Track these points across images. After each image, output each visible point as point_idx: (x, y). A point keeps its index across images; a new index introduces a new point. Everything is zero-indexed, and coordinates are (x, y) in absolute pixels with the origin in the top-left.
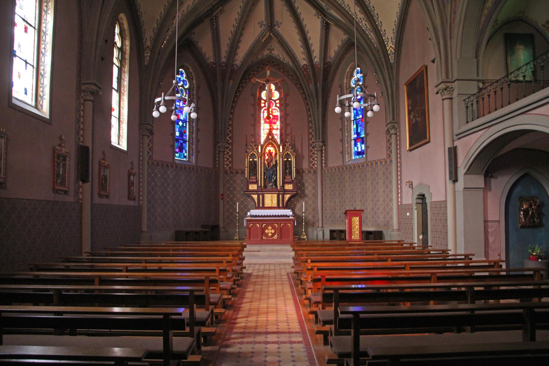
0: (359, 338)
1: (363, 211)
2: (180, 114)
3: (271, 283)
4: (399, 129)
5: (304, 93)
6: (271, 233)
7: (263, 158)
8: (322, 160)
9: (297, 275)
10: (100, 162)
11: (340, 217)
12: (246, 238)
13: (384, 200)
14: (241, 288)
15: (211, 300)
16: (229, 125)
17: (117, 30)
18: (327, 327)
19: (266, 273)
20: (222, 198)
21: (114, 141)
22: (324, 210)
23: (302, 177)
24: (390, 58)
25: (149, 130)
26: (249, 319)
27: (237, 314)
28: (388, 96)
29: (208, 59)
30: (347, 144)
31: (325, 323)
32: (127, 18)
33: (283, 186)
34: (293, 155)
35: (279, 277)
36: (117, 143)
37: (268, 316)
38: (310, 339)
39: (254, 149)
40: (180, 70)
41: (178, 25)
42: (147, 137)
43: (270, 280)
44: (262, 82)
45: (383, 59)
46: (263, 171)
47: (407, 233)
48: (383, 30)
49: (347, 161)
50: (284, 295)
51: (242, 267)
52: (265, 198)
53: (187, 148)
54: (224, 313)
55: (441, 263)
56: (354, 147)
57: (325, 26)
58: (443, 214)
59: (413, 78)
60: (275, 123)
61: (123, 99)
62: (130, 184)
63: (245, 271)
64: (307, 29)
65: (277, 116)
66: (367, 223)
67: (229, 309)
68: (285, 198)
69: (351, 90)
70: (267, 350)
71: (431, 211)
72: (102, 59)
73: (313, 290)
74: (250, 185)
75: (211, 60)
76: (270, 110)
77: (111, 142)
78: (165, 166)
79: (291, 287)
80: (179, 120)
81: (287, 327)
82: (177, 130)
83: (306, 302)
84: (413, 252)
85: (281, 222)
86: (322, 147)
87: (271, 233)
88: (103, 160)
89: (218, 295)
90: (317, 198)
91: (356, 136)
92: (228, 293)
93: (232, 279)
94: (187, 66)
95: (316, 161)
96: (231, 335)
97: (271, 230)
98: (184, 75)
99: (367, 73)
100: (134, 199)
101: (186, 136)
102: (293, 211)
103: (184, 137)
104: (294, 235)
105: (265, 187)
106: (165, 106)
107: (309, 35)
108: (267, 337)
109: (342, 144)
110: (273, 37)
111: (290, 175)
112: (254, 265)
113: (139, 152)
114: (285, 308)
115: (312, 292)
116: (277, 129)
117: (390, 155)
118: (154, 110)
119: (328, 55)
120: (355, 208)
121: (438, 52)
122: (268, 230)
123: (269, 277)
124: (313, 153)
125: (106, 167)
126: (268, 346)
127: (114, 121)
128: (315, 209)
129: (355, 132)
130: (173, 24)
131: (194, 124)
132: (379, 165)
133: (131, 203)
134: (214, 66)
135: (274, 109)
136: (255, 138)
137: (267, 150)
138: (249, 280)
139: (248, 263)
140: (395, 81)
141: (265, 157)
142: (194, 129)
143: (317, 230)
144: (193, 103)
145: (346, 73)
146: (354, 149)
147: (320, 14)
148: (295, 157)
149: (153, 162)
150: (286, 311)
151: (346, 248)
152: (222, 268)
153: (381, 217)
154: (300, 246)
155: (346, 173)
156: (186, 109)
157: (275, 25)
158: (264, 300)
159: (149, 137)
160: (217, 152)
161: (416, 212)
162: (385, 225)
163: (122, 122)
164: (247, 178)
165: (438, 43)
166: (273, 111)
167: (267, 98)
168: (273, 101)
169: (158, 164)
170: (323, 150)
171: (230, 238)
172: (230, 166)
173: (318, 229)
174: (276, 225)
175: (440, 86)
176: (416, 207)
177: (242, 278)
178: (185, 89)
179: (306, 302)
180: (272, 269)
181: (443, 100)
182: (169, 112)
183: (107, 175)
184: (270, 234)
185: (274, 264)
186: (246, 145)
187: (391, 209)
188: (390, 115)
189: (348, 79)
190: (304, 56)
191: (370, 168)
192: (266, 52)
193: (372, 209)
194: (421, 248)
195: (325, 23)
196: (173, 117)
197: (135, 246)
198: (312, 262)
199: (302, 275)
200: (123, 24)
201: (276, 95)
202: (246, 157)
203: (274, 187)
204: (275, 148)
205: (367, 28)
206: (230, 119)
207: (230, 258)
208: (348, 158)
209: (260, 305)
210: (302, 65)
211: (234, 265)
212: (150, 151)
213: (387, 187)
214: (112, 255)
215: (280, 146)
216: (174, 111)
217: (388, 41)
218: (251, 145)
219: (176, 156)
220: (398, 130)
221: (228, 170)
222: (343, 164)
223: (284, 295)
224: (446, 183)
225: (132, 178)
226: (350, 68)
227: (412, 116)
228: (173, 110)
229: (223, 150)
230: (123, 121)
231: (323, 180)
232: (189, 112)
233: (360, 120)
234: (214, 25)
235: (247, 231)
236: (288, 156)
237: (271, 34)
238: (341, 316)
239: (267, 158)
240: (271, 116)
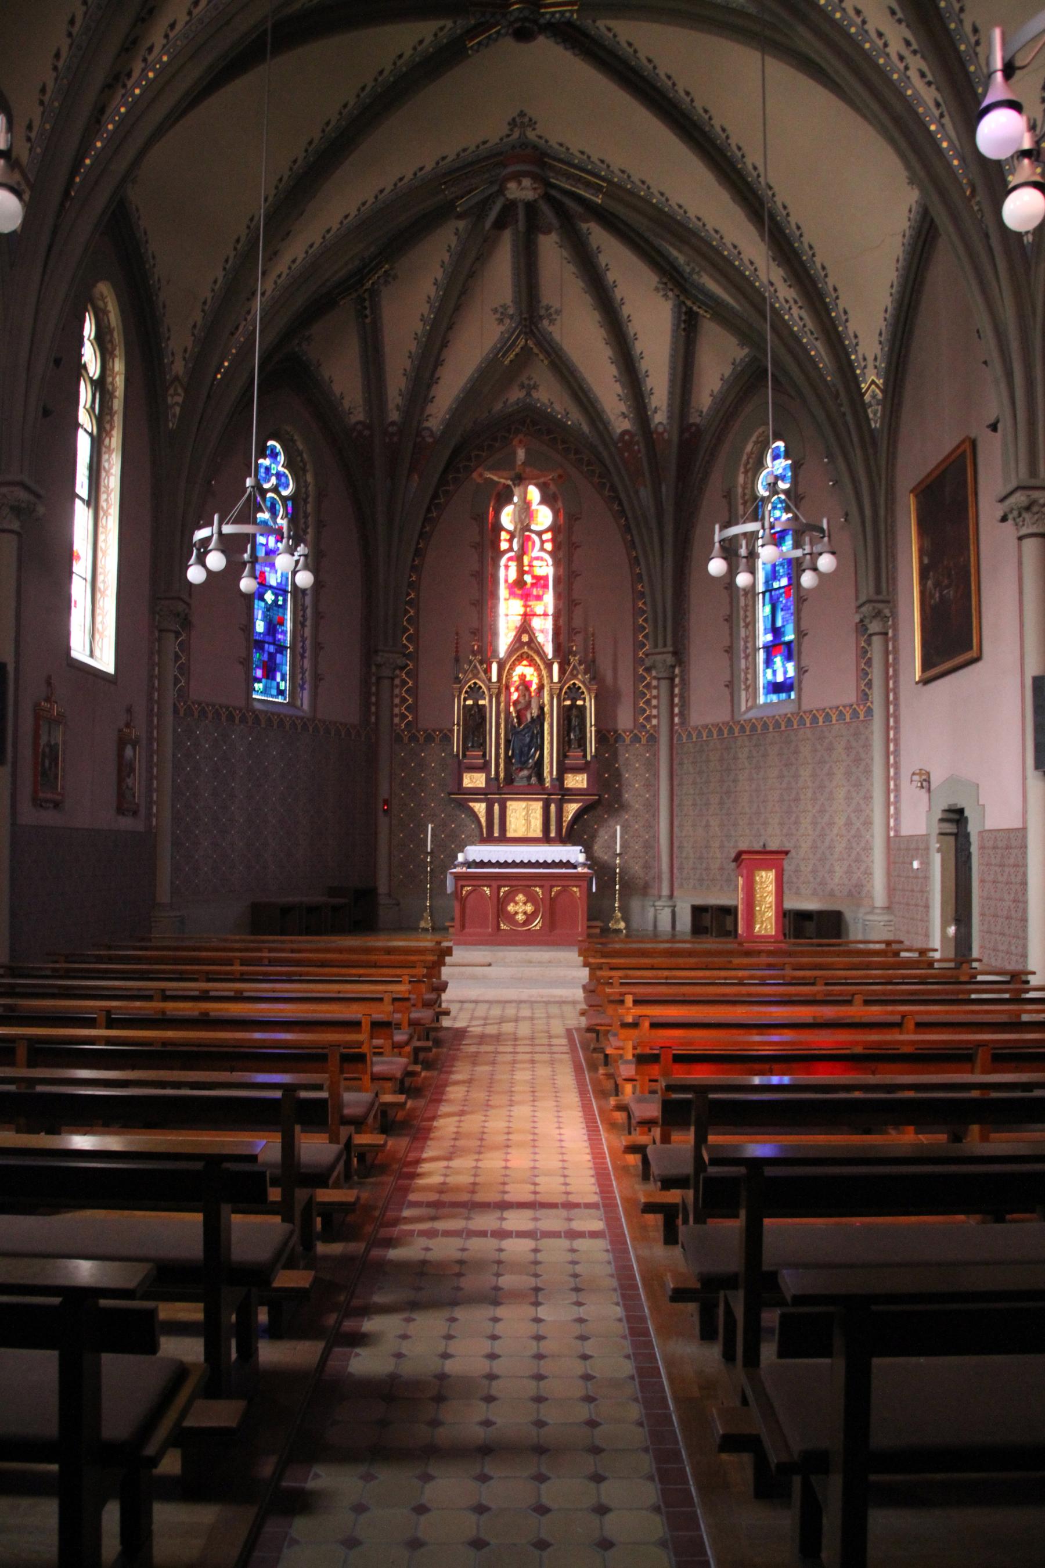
0: (761, 1225)
1: (787, 853)
2: (267, 569)
3: (520, 1057)
4: (893, 621)
5: (623, 512)
6: (525, 913)
7: (502, 698)
8: (672, 705)
9: (594, 1035)
10: (37, 705)
11: (721, 869)
12: (453, 926)
13: (849, 824)
14: (435, 1073)
15: (346, 1111)
16: (407, 603)
17: (89, 329)
18: (674, 1196)
19: (507, 1028)
20: (384, 810)
21: (79, 650)
22: (675, 849)
23: (615, 756)
24: (871, 416)
25: (178, 615)
26: (453, 1164)
27: (422, 1149)
28: (863, 523)
29: (351, 413)
30: (743, 661)
31: (668, 1183)
32: (117, 295)
33: (560, 778)
34: (589, 690)
35: (545, 1041)
36: (88, 652)
37: (509, 1157)
38: (624, 1225)
39: (479, 672)
40: (270, 443)
41: (261, 319)
42: (172, 636)
43: (519, 1049)
44: (503, 481)
45: (849, 418)
46: (502, 736)
47: (912, 919)
48: (852, 335)
49: (743, 708)
50: (556, 1093)
51: (438, 1010)
52: (509, 812)
53: (288, 668)
54: (384, 1145)
55: (1000, 1013)
56: (764, 670)
57: (685, 321)
58: (1016, 866)
59: (937, 472)
60: (539, 598)
61: (105, 527)
62: (124, 769)
63: (446, 1022)
64: (632, 329)
65: (546, 578)
66: (798, 888)
67: (399, 1135)
68: (565, 814)
69: (755, 510)
70: (503, 1256)
71: (982, 856)
72: (46, 413)
73: (638, 1084)
74: (465, 775)
75: (359, 416)
76: (526, 560)
77: (68, 649)
78: (223, 718)
79: (578, 1069)
80: (263, 585)
81: (563, 1188)
82: (260, 616)
83: (619, 1117)
84: (927, 976)
85: (554, 883)
86: (673, 667)
87: (525, 913)
88: (48, 699)
89: (366, 1097)
90: (655, 814)
91: (769, 637)
92: (397, 1089)
93: (408, 1049)
94: (288, 433)
95: (655, 707)
96: (401, 1210)
97: (525, 903)
98: (281, 458)
99: (804, 458)
100: (135, 813)
101: (284, 633)
102: (588, 851)
103: (280, 636)
104: (588, 920)
105: (510, 780)
106: (223, 552)
107: (638, 347)
108: (503, 1219)
109: (731, 659)
110: (536, 350)
111: (580, 746)
112: (471, 1006)
113: (151, 677)
114: (558, 1131)
115: (634, 1087)
116: (545, 615)
117: (866, 694)
118: (191, 562)
119: (693, 404)
120: (764, 845)
121: (1006, 401)
122: (516, 903)
123: (516, 1039)
124: (648, 686)
125: (58, 720)
126: (507, 1244)
127: (79, 590)
128: (650, 845)
129: (769, 626)
130: (249, 312)
131: (308, 600)
132: (834, 722)
133: (126, 823)
134: (367, 433)
135: (537, 558)
136: (481, 639)
137: (514, 674)
138: (458, 1049)
139: (458, 999)
140: (883, 482)
141: (510, 694)
142: (309, 611)
143: (654, 906)
144: (302, 545)
145: (745, 457)
146: (764, 675)
147: (670, 286)
148: (596, 697)
149: (189, 707)
150: (561, 1141)
151: (736, 961)
152: (378, 1016)
153: (839, 871)
154: (604, 955)
155: (739, 743)
156: (284, 562)
157: (541, 318)
158: (500, 1107)
159: (178, 634)
160: (374, 679)
161: (937, 859)
162: (850, 894)
163: (103, 593)
164: (458, 755)
165: (1009, 375)
166: (535, 563)
167: (515, 528)
168: (533, 536)
169: (203, 713)
170: (676, 676)
171: (406, 926)
172: (410, 718)
173: (657, 904)
174: (537, 889)
175: (1012, 500)
176: (938, 845)
177: (438, 1043)
178: (284, 499)
179: (619, 1117)
180: (525, 1018)
181: (1020, 538)
182: (234, 570)
183: (57, 744)
184: (520, 917)
185: (532, 1003)
186: (457, 660)
187: (868, 849)
188: (867, 584)
189: (750, 474)
190: (623, 408)
191: (808, 731)
192: (515, 395)
193: (814, 847)
194: (952, 965)
195: (686, 313)
196: (247, 584)
197: (135, 948)
198: (636, 1002)
199: (609, 1040)
200: (106, 312)
201: (544, 517)
202: (456, 694)
203: (534, 780)
204: (538, 669)
205: (805, 329)
206: (411, 585)
207: (402, 989)
208: (747, 701)
209: (486, 1124)
210: (619, 431)
211: (414, 1005)
212: (182, 675)
213: (858, 785)
214: (68, 974)
215: (552, 663)
216: (248, 566)
217: (865, 367)
218: (471, 662)
219: (257, 689)
220: (890, 623)
221: (403, 731)
222: (733, 717)
223: (556, 1093)
224: (1024, 778)
225: (129, 752)
226: (756, 443)
227: (930, 583)
228: (245, 564)
229: (390, 675)
230: (105, 590)
231: (675, 762)
232: (292, 568)
233: (782, 590)
234: (366, 316)
235: (456, 905)
236: (574, 692)
237: (530, 343)
238: (712, 1170)
239: (515, 696)
240: (528, 578)
